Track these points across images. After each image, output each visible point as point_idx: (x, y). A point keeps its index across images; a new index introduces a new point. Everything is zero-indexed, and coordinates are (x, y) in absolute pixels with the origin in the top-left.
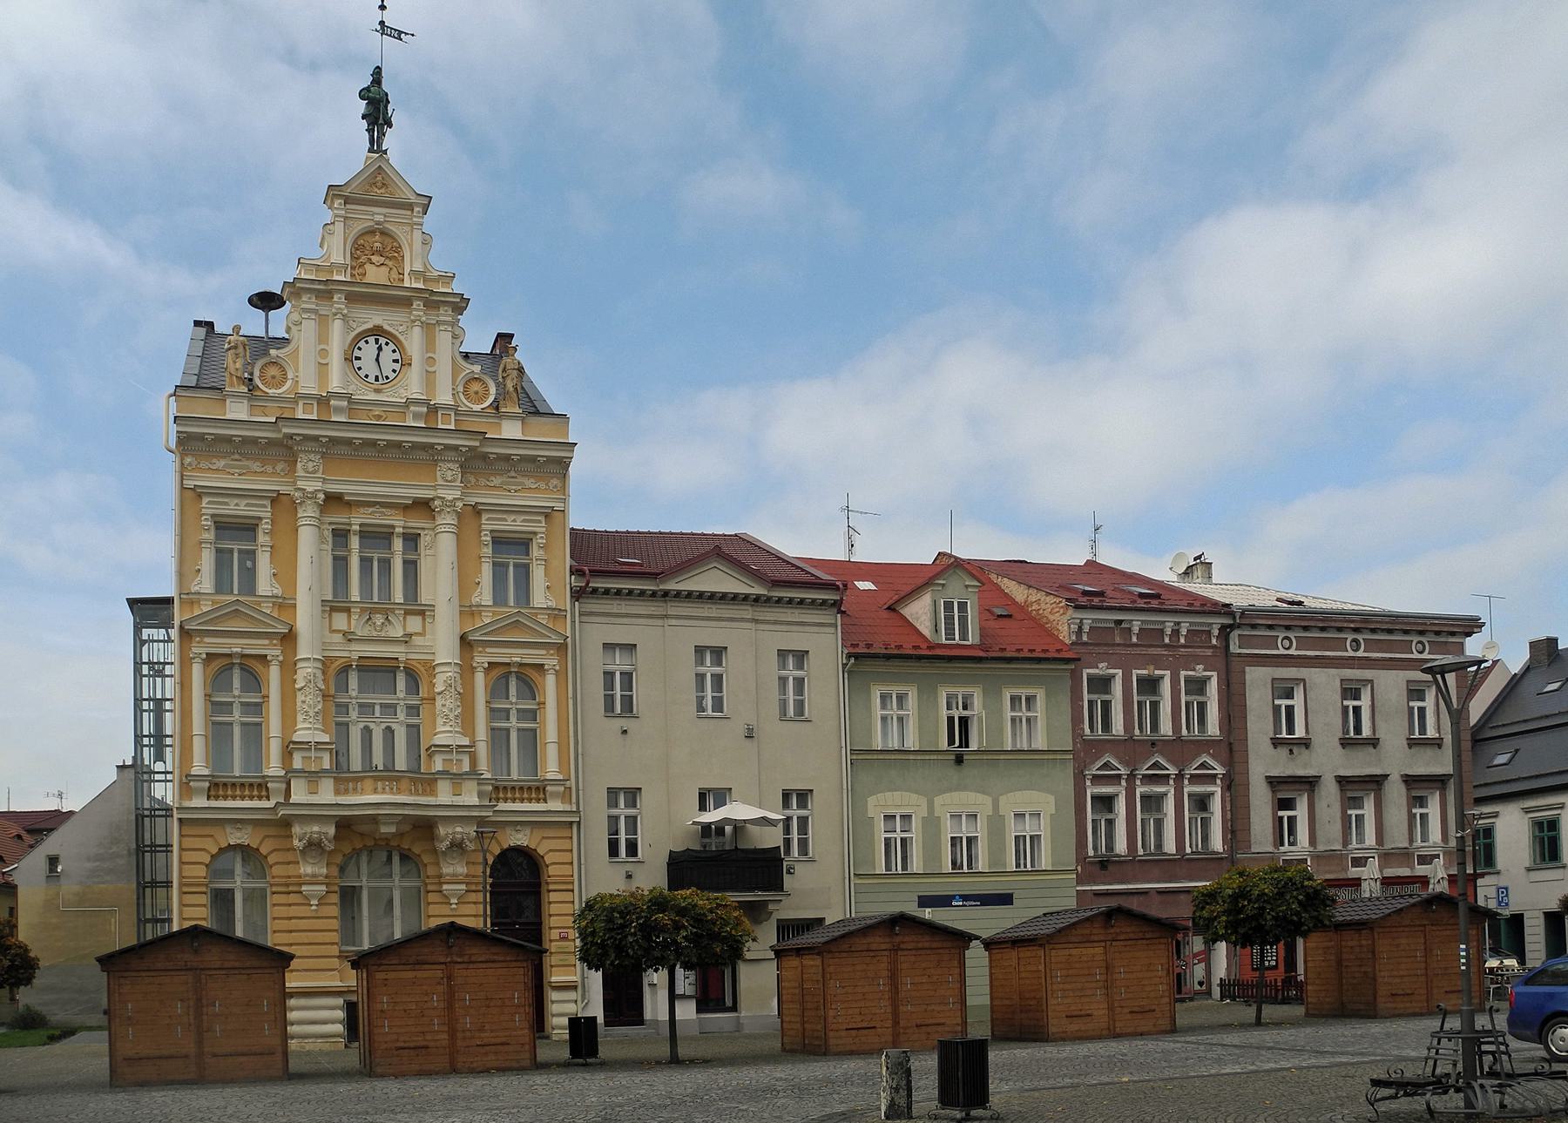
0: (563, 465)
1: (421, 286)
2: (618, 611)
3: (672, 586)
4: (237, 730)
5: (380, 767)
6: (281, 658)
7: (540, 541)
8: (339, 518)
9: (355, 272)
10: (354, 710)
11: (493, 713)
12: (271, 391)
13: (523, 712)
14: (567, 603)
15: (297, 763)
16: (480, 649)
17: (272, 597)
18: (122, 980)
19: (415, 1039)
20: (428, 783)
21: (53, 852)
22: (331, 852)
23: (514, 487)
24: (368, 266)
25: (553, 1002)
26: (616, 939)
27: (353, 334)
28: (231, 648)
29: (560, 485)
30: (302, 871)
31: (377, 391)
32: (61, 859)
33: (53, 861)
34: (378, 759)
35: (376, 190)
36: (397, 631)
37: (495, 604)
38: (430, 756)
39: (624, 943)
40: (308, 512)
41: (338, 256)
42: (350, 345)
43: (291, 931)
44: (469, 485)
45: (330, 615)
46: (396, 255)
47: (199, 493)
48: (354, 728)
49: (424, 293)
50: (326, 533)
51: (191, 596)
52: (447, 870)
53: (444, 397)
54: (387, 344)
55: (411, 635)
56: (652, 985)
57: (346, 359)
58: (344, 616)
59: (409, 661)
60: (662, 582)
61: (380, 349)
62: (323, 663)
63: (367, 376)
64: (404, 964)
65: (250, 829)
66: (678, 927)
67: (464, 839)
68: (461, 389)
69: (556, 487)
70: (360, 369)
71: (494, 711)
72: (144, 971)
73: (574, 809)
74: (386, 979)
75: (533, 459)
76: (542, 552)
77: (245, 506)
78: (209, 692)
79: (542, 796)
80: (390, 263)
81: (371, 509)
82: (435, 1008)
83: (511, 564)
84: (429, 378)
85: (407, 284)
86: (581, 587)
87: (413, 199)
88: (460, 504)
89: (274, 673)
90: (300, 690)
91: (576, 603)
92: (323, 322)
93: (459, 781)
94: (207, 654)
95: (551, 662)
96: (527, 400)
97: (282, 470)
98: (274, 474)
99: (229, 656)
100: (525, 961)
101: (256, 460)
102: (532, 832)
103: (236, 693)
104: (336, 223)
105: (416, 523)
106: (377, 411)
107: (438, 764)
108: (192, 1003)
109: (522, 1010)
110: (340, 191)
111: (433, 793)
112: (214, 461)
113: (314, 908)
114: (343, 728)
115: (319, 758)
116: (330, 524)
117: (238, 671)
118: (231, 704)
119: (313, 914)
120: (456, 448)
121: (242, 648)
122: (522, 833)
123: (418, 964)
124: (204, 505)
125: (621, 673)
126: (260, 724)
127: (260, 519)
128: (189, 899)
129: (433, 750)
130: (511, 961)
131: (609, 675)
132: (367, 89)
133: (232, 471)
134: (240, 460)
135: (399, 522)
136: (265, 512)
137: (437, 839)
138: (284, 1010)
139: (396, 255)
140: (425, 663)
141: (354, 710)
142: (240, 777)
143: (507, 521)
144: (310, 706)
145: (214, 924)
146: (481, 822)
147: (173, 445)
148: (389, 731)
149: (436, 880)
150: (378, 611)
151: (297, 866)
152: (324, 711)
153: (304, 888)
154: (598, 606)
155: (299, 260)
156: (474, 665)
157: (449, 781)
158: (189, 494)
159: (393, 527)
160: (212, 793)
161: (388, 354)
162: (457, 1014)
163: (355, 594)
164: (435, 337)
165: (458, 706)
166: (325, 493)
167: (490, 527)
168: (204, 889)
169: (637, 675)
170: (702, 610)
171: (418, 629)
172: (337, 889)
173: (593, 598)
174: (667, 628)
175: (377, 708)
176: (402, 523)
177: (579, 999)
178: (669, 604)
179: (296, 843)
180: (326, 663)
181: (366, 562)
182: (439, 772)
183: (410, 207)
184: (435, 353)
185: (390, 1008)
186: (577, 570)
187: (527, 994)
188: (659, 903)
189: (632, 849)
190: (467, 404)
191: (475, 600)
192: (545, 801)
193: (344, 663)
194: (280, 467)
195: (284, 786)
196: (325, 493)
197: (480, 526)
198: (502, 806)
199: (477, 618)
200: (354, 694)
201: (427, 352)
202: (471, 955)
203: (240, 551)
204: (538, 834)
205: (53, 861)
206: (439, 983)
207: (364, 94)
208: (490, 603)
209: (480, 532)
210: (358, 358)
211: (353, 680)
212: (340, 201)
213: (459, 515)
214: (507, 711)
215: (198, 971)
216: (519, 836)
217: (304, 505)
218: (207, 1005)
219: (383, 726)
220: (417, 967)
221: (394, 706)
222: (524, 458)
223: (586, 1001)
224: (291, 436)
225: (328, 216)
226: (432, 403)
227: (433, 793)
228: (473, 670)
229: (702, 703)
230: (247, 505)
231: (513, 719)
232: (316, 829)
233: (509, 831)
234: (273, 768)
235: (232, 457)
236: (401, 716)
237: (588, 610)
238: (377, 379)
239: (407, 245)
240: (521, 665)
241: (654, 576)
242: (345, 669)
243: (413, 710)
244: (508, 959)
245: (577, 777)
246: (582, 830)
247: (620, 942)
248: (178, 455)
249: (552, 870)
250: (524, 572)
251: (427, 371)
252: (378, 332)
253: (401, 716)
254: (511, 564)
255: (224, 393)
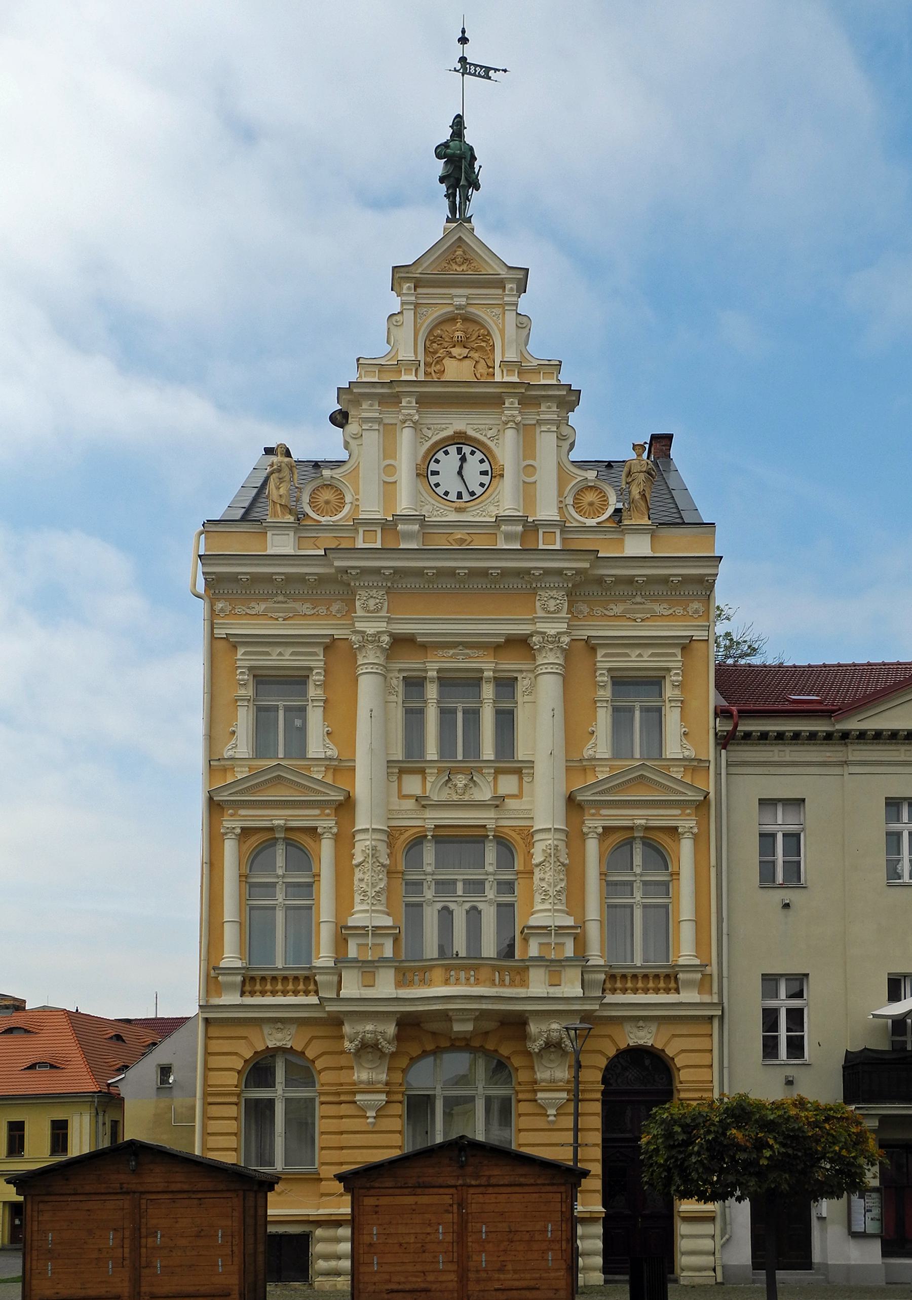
0: (706, 585)
1: (515, 379)
2: (905, 759)
3: (853, 724)
4: (638, 913)
5: (463, 953)
6: (335, 830)
7: (317, 678)
8: (411, 663)
9: (430, 370)
10: (429, 888)
11: (610, 887)
12: (323, 520)
13: (294, 886)
14: (710, 751)
15: (353, 951)
16: (593, 811)
17: (326, 759)
18: (41, 1206)
19: (414, 1279)
20: (520, 973)
21: (165, 1061)
22: (393, 1055)
23: (639, 616)
24: (447, 362)
25: (683, 1237)
26: (677, 1160)
27: (428, 445)
28: (633, 820)
29: (702, 609)
30: (355, 1077)
31: (459, 510)
32: (174, 1069)
33: (165, 1071)
34: (460, 945)
35: (455, 267)
36: (484, 793)
37: (616, 755)
38: (526, 940)
39: (686, 1164)
40: (369, 658)
41: (406, 353)
42: (425, 457)
43: (342, 1148)
44: (581, 616)
45: (400, 779)
46: (484, 344)
47: (233, 643)
48: (429, 909)
49: (520, 388)
50: (394, 682)
51: (222, 763)
52: (542, 1075)
53: (547, 511)
54: (473, 453)
55: (503, 798)
56: (821, 1219)
57: (418, 475)
58: (417, 778)
59: (499, 829)
60: (838, 721)
61: (463, 459)
62: (389, 835)
63: (446, 493)
64: (401, 1187)
65: (293, 1029)
66: (761, 1145)
67: (562, 1039)
68: (570, 500)
69: (696, 612)
70: (437, 485)
71: (612, 885)
72: (70, 1194)
73: (716, 1000)
74: (377, 1206)
75: (665, 580)
76: (677, 692)
77: (650, 656)
78: (604, 870)
79: (672, 985)
80: (476, 355)
81: (451, 652)
82: (440, 1242)
83: (637, 708)
84: (528, 491)
85: (498, 378)
86: (728, 731)
87: (504, 273)
88: (566, 639)
89: (327, 848)
90: (358, 866)
91: (723, 751)
92: (389, 432)
93: (558, 969)
94: (604, 828)
95: (687, 823)
96: (675, 510)
97: (338, 611)
98: (329, 616)
99: (271, 829)
100: (561, 1184)
101: (305, 601)
102: (658, 1030)
103: (280, 872)
104: (404, 311)
105: (510, 664)
106: (459, 534)
107: (534, 950)
108: (127, 1233)
109: (557, 1246)
110: (407, 273)
111: (524, 983)
112: (612, 606)
113: (370, 1120)
114: (415, 910)
115: (379, 945)
116: (400, 671)
117: (641, 846)
118: (274, 885)
119: (370, 1128)
120: (559, 572)
121: (647, 820)
122: (646, 1030)
123: (419, 1187)
124: (239, 657)
125: (784, 834)
126: (309, 908)
127: (311, 669)
128: (214, 1111)
129: (530, 932)
130: (544, 1185)
131: (767, 839)
132: (446, 145)
133: (274, 615)
134: (285, 602)
135: (487, 665)
136: (316, 661)
137: (530, 1038)
138: (573, 1237)
139: (484, 344)
140: (520, 830)
141: (429, 888)
142: (284, 969)
143: (629, 656)
144: (549, 885)
145: (484, 1138)
146: (586, 1017)
147: (201, 587)
148: (474, 914)
149: (529, 1088)
150: (459, 771)
151: (350, 1071)
152: (389, 889)
153: (358, 1097)
154: (754, 754)
155: (358, 360)
156: (585, 830)
157: (356, 971)
158: (221, 645)
159: (481, 671)
160: (247, 988)
161: (473, 465)
162: (470, 1249)
163: (432, 752)
164: (535, 440)
165: (561, 880)
166: (391, 635)
167: (247, 664)
168: (234, 1099)
169: (805, 836)
170: (894, 753)
171: (515, 791)
172: (399, 1097)
173: (747, 744)
174: (846, 777)
175: (460, 886)
176: (492, 666)
177: (718, 1232)
178: (850, 748)
179: (347, 1044)
180: (391, 835)
181: (446, 715)
182: (532, 959)
183: (500, 284)
184: (535, 460)
185: (380, 1241)
186: (722, 711)
187: (564, 1226)
188: (828, 1115)
189: (796, 1047)
190: (576, 518)
191: (588, 753)
192: (677, 991)
193: (414, 834)
194: (335, 607)
195: (336, 978)
196: (391, 635)
197: (595, 665)
198: (610, 998)
199: (229, 775)
200: (429, 869)
201: (384, 460)
202: (489, 1177)
203: (287, 709)
204: (668, 1030)
205: (165, 1071)
206: (447, 1211)
207: (441, 151)
208: (492, 758)
209: (595, 672)
210: (435, 473)
211: (429, 854)
212: (408, 285)
213: (567, 653)
214: (631, 884)
215: (136, 1195)
216: (641, 1033)
217: (364, 651)
218: (147, 1237)
219: (467, 906)
220: (419, 1191)
221: (482, 883)
222: (651, 580)
223: (727, 1236)
224: (345, 571)
225: (395, 302)
226: (530, 519)
227: (524, 983)
228: (583, 837)
229: (896, 869)
230: (293, 654)
231: (638, 895)
232: (370, 1027)
233: (628, 1027)
234: (324, 957)
235: (633, 600)
236: (490, 893)
237: (739, 760)
238: (460, 495)
239: (497, 332)
240: (647, 828)
241: (828, 714)
242: (418, 841)
243: (507, 887)
244: (539, 1182)
245: (720, 964)
246: (726, 1026)
247: (682, 1163)
248: (207, 600)
249: (684, 1075)
250: (655, 716)
251: (524, 482)
252: (460, 440)
253: (490, 893)
254: (637, 708)
255: (264, 524)
